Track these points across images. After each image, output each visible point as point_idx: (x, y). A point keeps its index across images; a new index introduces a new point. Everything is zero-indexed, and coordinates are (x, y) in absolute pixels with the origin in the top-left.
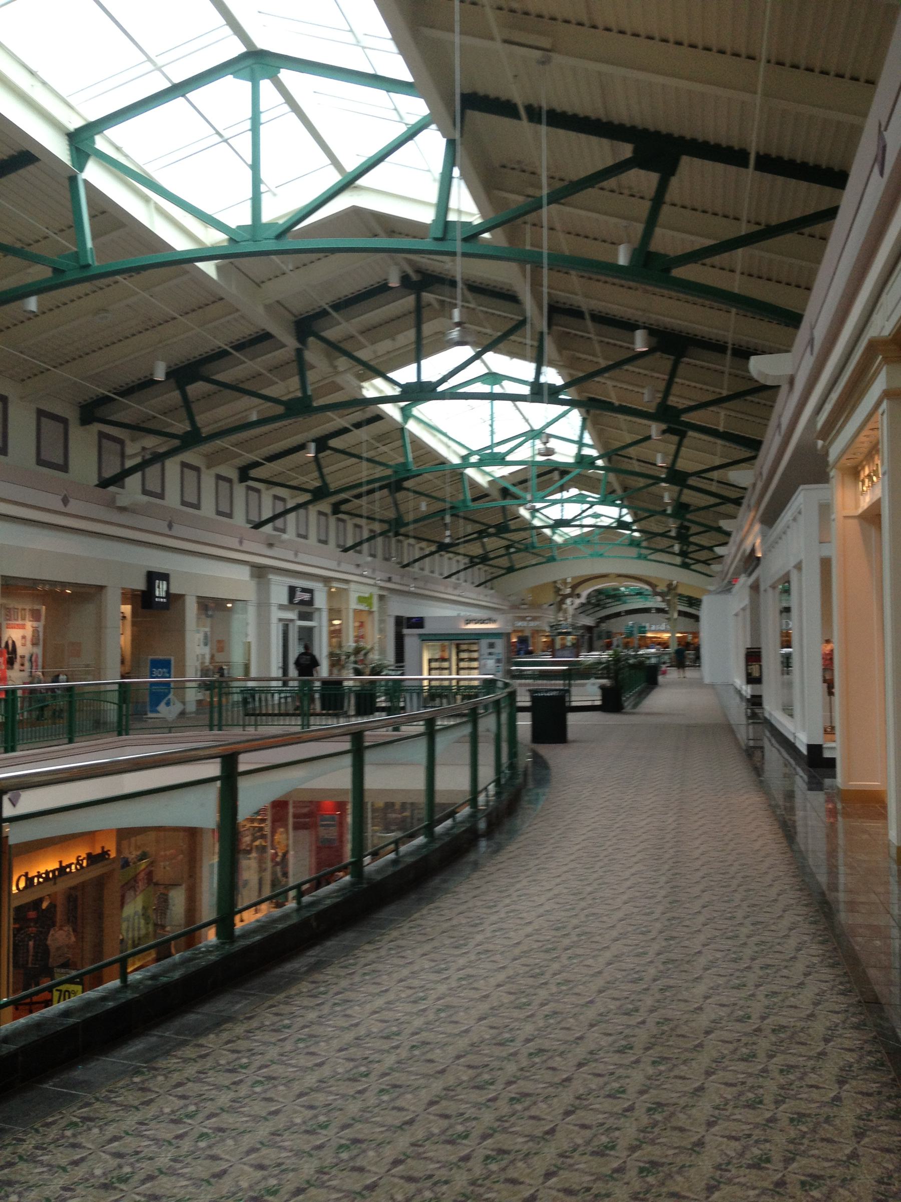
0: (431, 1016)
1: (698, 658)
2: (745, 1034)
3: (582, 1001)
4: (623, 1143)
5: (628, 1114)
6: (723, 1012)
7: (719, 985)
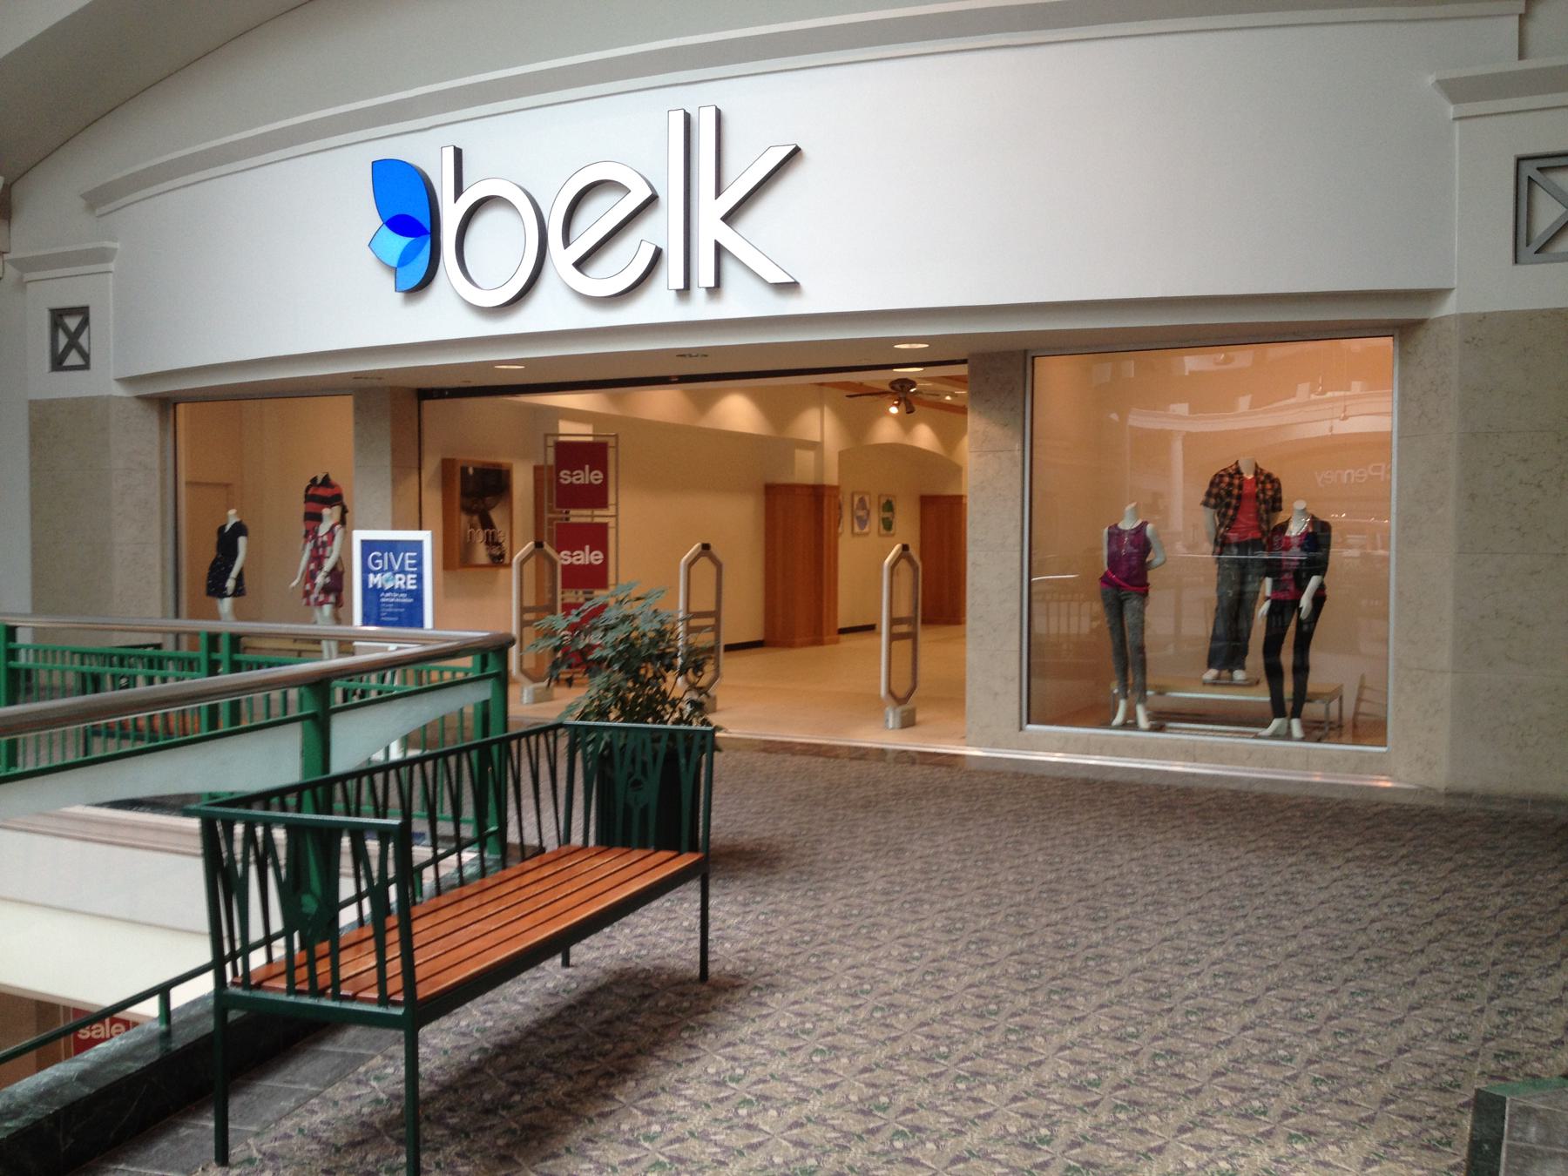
0: (1040, 998)
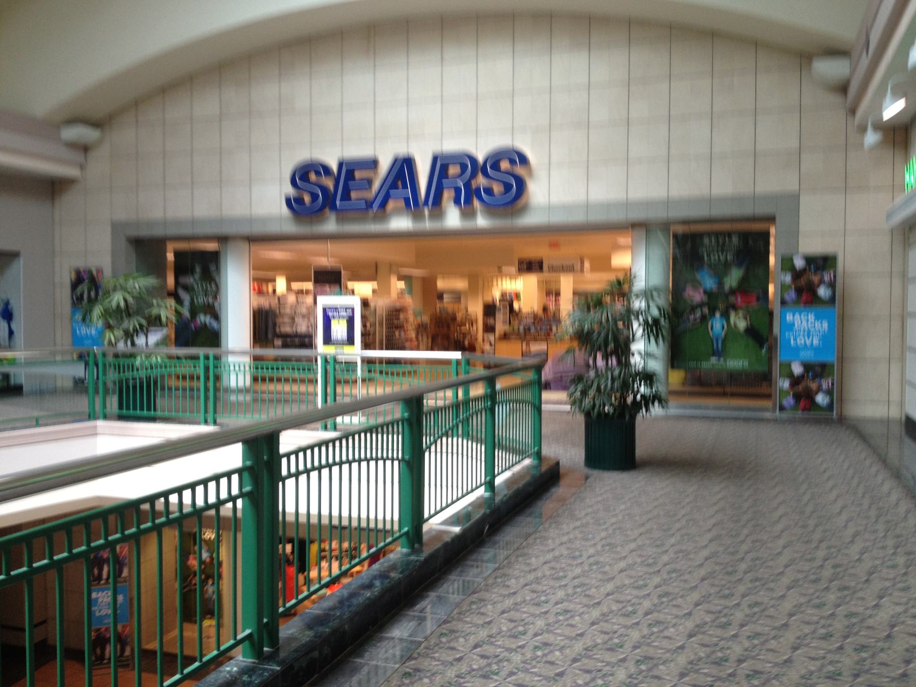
1: (75, 285)
2: (829, 652)
3: (687, 586)
4: (733, 658)
5: (731, 678)
6: (807, 629)
7: (811, 673)
